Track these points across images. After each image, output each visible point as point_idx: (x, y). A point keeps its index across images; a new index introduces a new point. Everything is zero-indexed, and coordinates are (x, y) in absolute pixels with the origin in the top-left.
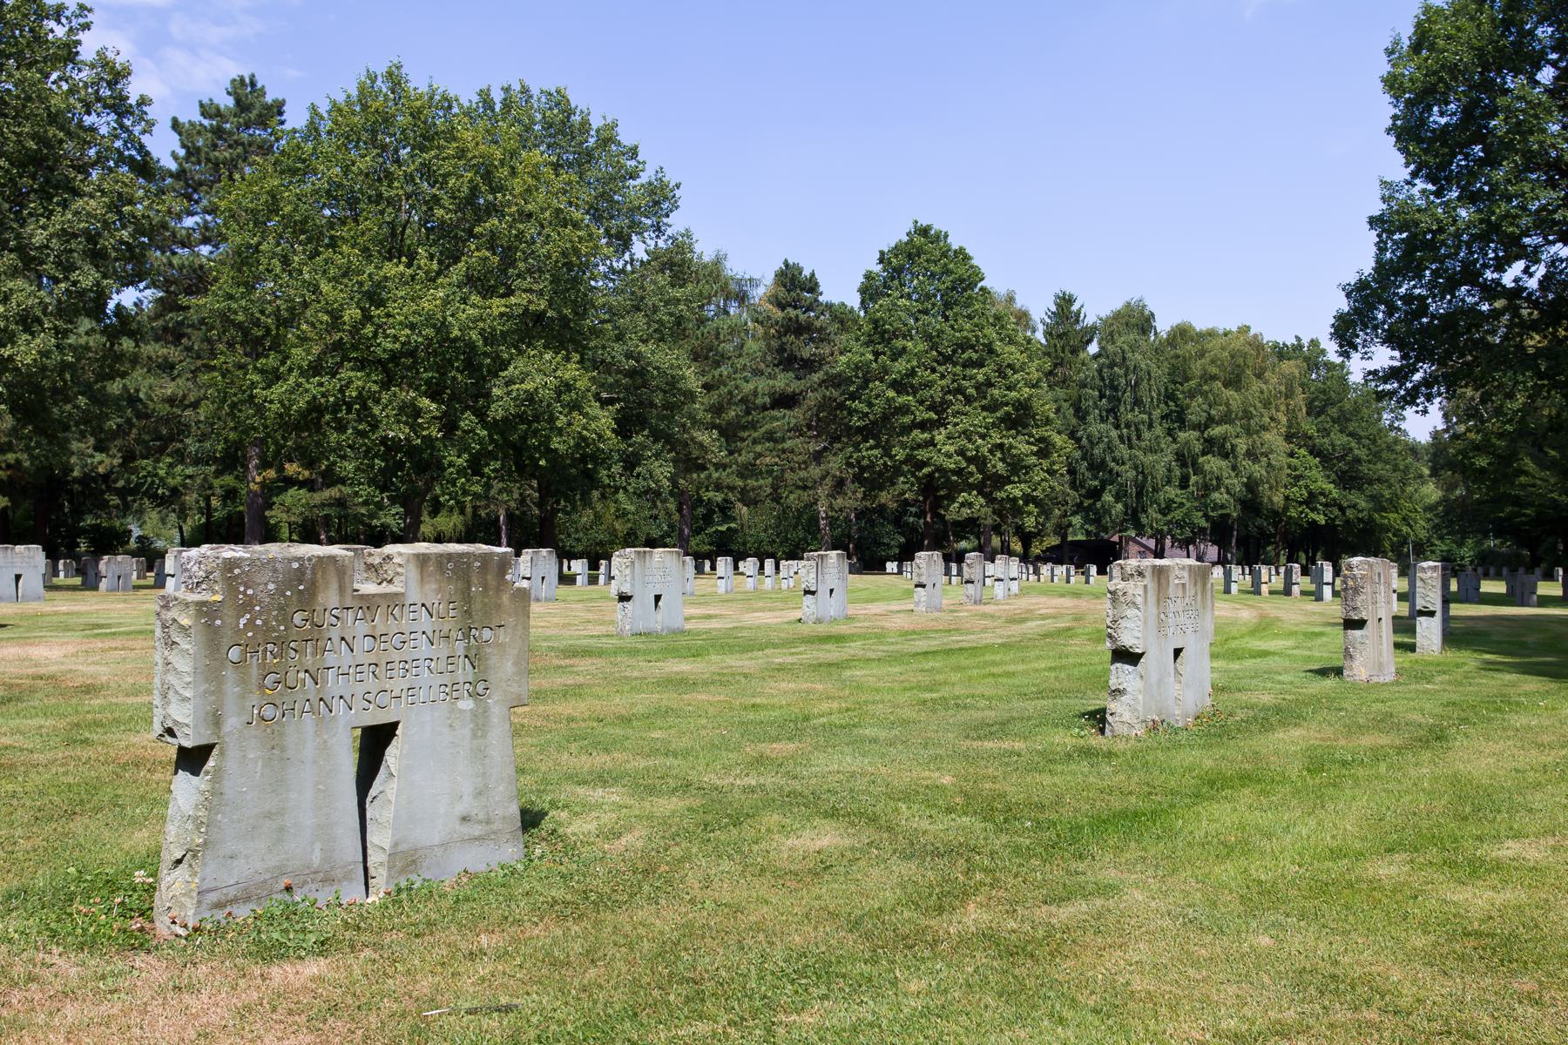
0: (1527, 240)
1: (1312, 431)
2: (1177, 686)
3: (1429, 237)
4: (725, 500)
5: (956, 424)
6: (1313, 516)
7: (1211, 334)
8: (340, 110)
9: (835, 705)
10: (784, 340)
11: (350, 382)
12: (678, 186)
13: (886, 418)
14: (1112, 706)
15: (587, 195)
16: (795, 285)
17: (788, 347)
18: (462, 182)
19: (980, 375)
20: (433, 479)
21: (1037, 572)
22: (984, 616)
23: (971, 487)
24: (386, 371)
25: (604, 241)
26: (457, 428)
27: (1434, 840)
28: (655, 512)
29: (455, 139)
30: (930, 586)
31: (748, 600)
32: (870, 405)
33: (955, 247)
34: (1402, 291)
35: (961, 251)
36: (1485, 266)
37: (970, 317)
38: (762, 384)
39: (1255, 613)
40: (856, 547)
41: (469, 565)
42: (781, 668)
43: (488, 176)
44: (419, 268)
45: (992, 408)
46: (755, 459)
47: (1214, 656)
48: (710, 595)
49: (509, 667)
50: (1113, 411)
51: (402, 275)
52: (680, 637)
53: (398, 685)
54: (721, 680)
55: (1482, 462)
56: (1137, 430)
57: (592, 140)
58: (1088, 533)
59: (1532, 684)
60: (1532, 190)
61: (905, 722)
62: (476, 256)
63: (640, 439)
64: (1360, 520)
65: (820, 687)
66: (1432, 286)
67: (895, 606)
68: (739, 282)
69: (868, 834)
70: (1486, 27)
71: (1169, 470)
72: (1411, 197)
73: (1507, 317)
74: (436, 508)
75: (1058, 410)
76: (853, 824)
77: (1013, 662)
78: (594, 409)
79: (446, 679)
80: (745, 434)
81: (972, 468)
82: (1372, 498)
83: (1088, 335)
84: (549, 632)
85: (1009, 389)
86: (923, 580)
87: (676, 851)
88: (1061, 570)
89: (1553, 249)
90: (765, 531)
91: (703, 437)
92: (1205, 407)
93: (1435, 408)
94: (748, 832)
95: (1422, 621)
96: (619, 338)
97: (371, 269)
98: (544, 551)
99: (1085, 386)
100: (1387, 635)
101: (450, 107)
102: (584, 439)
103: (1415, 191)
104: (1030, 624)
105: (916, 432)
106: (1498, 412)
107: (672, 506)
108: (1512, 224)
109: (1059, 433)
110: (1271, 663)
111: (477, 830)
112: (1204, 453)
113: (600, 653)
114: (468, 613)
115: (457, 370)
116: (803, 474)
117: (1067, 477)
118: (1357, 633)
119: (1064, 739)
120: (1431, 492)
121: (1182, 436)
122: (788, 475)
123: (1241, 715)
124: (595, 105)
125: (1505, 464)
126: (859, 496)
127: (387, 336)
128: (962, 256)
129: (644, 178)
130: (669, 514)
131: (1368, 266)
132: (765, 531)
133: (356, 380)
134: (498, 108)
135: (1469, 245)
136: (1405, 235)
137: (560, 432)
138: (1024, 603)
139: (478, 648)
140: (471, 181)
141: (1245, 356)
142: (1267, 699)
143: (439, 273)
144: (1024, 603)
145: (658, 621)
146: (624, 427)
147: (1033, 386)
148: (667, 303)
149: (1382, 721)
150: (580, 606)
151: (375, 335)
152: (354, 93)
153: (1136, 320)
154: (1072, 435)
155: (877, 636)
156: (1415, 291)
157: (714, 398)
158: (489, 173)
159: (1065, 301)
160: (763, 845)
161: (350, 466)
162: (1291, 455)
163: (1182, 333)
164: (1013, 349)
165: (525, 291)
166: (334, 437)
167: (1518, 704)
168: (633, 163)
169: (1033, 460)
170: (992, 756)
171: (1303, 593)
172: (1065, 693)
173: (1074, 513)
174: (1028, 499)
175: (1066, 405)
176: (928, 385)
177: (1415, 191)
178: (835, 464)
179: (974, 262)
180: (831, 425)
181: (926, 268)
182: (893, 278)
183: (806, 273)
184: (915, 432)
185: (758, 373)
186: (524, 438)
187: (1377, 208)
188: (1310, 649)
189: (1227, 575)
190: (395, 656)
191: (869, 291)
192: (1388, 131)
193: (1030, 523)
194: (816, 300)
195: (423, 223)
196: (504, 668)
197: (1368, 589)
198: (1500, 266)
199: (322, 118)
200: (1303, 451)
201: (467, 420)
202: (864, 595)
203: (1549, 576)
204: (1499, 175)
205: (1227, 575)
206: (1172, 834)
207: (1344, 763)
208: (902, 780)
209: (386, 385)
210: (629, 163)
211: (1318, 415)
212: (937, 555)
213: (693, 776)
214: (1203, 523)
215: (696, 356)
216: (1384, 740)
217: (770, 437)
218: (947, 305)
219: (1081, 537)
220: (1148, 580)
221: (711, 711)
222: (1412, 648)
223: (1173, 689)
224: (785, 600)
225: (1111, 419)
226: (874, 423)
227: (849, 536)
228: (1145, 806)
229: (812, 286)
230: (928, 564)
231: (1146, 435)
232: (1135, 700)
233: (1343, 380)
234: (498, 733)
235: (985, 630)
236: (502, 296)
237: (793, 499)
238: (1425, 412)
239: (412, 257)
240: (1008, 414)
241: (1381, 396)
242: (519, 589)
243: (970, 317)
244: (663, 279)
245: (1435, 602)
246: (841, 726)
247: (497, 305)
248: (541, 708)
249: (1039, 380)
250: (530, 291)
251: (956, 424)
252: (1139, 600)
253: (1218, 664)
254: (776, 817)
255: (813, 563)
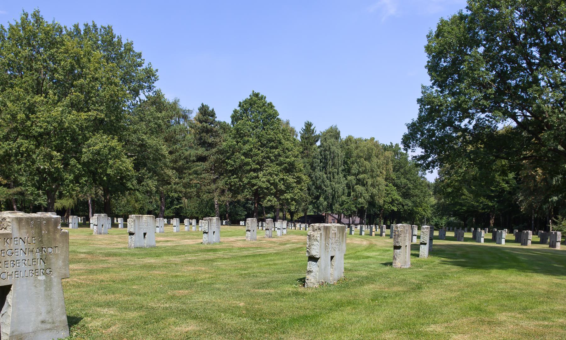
0: (470, 111)
1: (394, 177)
2: (332, 270)
3: (437, 107)
4: (179, 196)
5: (267, 170)
6: (393, 208)
7: (360, 140)
8: (13, 29)
9: (207, 276)
10: (202, 135)
11: (22, 144)
12: (157, 70)
13: (240, 167)
14: (308, 277)
15: (120, 72)
16: (206, 113)
17: (203, 138)
18: (67, 63)
19: (276, 152)
20: (59, 185)
21: (295, 226)
22: (271, 242)
23: (272, 194)
24: (37, 141)
25: (128, 92)
26: (69, 165)
27: (408, 325)
28: (151, 200)
29: (64, 45)
30: (252, 231)
31: (184, 235)
32: (235, 162)
33: (268, 102)
34: (427, 127)
35: (270, 104)
36: (456, 120)
37: (273, 129)
38: (193, 152)
39: (368, 242)
40: (229, 216)
41: (41, 222)
42: (190, 262)
43: (78, 61)
44: (50, 98)
45: (280, 164)
46: (190, 181)
47: (345, 259)
48: (171, 233)
49: (60, 263)
50: (324, 167)
51: (43, 101)
52: (153, 249)
53: (11, 270)
54: (165, 266)
55: (450, 190)
56: (333, 175)
57: (122, 49)
58: (315, 212)
59: (455, 269)
60: (473, 92)
61: (232, 282)
62: (74, 94)
63: (143, 171)
64: (409, 210)
65: (203, 269)
66: (437, 126)
67: (239, 238)
68: (184, 111)
69: (207, 325)
70: (462, 30)
71: (344, 190)
72: (432, 92)
73: (462, 138)
74: (61, 196)
75: (304, 167)
76: (202, 321)
77: (278, 260)
78: (124, 158)
79: (32, 268)
80: (186, 171)
81: (272, 187)
82: (413, 202)
83: (317, 139)
84: (102, 246)
85: (287, 157)
86: (249, 229)
87: (131, 333)
88: (303, 225)
89: (479, 115)
90: (194, 208)
91: (170, 172)
92: (358, 168)
93: (436, 170)
94: (161, 325)
95: (422, 247)
96: (135, 132)
97: (28, 98)
98: (103, 215)
99: (315, 158)
100: (408, 251)
101: (61, 31)
102: (121, 170)
103: (434, 90)
104: (288, 245)
105: (252, 173)
106: (456, 173)
107: (158, 198)
108: (466, 104)
109: (305, 175)
110: (369, 260)
111: (49, 326)
112: (356, 184)
113: (120, 255)
114: (41, 242)
115: (68, 141)
116: (209, 187)
117: (307, 191)
118: (398, 251)
119: (289, 288)
120: (433, 200)
121: (349, 178)
122: (203, 187)
123: (354, 279)
124: (124, 33)
125: (457, 192)
126: (230, 196)
127: (37, 126)
128: (271, 106)
129: (144, 66)
130: (156, 201)
131: (416, 118)
132: (194, 208)
133: (26, 144)
134: (82, 32)
135: (451, 111)
136: (429, 106)
137: (111, 167)
138: (287, 238)
139: (46, 256)
140: (71, 63)
141: (372, 149)
142: (364, 274)
143: (58, 101)
144: (287, 238)
145: (145, 243)
146: (137, 166)
147: (296, 157)
148: (154, 118)
149: (402, 282)
150: (117, 236)
151: (32, 126)
152: (19, 22)
153: (334, 133)
154: (309, 176)
155: (230, 249)
156: (431, 128)
157: (173, 157)
158: (78, 60)
159: (309, 125)
160: (166, 330)
161: (24, 179)
162: (387, 186)
163: (349, 139)
164: (288, 142)
165: (95, 110)
166: (16, 167)
167: (448, 276)
168: (139, 60)
169: (295, 185)
170: (261, 295)
171: (386, 235)
172: (294, 271)
173: (309, 204)
174: (293, 199)
175: (307, 164)
176: (256, 155)
177: (434, 90)
178: (221, 183)
179: (275, 108)
180: (219, 169)
181: (256, 110)
182: (244, 113)
183: (210, 109)
184: (247, 171)
185: (191, 147)
186: (96, 169)
187: (420, 96)
188: (384, 256)
189: (361, 228)
190: (9, 259)
191: (235, 117)
192: (426, 67)
193: (293, 208)
194: (214, 120)
195: (52, 79)
196: (58, 263)
197: (403, 235)
198: (460, 121)
199: (5, 31)
200: (391, 185)
201: (73, 161)
202: (229, 234)
203: (469, 231)
204: (463, 86)
205: (361, 228)
206: (318, 324)
207: (385, 297)
208: (224, 305)
209: (37, 147)
210: (138, 60)
211: (397, 171)
212: (255, 219)
213: (145, 303)
214: (355, 209)
215: (166, 140)
216: (401, 289)
217: (196, 173)
218: (265, 124)
219: (312, 214)
220: (322, 231)
221: (159, 278)
222: (418, 256)
223: (330, 270)
224: (198, 235)
225: (324, 171)
226: (236, 169)
227: (226, 211)
228: (311, 313)
229: (213, 114)
230: (251, 223)
231: (336, 177)
232: (315, 274)
233: (406, 159)
234: (56, 290)
235: (270, 247)
236: (85, 112)
237: (205, 197)
238: (432, 172)
239: (47, 94)
240: (286, 167)
241: (417, 165)
242: (64, 232)
243: (273, 129)
244: (153, 109)
245: (426, 239)
246: (208, 284)
247: (83, 115)
248: (91, 276)
249: (298, 155)
250: (98, 110)
251: (267, 170)
252: (318, 239)
253: (347, 261)
254: (173, 319)
255: (207, 221)
